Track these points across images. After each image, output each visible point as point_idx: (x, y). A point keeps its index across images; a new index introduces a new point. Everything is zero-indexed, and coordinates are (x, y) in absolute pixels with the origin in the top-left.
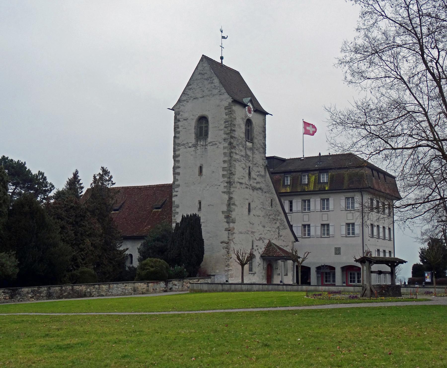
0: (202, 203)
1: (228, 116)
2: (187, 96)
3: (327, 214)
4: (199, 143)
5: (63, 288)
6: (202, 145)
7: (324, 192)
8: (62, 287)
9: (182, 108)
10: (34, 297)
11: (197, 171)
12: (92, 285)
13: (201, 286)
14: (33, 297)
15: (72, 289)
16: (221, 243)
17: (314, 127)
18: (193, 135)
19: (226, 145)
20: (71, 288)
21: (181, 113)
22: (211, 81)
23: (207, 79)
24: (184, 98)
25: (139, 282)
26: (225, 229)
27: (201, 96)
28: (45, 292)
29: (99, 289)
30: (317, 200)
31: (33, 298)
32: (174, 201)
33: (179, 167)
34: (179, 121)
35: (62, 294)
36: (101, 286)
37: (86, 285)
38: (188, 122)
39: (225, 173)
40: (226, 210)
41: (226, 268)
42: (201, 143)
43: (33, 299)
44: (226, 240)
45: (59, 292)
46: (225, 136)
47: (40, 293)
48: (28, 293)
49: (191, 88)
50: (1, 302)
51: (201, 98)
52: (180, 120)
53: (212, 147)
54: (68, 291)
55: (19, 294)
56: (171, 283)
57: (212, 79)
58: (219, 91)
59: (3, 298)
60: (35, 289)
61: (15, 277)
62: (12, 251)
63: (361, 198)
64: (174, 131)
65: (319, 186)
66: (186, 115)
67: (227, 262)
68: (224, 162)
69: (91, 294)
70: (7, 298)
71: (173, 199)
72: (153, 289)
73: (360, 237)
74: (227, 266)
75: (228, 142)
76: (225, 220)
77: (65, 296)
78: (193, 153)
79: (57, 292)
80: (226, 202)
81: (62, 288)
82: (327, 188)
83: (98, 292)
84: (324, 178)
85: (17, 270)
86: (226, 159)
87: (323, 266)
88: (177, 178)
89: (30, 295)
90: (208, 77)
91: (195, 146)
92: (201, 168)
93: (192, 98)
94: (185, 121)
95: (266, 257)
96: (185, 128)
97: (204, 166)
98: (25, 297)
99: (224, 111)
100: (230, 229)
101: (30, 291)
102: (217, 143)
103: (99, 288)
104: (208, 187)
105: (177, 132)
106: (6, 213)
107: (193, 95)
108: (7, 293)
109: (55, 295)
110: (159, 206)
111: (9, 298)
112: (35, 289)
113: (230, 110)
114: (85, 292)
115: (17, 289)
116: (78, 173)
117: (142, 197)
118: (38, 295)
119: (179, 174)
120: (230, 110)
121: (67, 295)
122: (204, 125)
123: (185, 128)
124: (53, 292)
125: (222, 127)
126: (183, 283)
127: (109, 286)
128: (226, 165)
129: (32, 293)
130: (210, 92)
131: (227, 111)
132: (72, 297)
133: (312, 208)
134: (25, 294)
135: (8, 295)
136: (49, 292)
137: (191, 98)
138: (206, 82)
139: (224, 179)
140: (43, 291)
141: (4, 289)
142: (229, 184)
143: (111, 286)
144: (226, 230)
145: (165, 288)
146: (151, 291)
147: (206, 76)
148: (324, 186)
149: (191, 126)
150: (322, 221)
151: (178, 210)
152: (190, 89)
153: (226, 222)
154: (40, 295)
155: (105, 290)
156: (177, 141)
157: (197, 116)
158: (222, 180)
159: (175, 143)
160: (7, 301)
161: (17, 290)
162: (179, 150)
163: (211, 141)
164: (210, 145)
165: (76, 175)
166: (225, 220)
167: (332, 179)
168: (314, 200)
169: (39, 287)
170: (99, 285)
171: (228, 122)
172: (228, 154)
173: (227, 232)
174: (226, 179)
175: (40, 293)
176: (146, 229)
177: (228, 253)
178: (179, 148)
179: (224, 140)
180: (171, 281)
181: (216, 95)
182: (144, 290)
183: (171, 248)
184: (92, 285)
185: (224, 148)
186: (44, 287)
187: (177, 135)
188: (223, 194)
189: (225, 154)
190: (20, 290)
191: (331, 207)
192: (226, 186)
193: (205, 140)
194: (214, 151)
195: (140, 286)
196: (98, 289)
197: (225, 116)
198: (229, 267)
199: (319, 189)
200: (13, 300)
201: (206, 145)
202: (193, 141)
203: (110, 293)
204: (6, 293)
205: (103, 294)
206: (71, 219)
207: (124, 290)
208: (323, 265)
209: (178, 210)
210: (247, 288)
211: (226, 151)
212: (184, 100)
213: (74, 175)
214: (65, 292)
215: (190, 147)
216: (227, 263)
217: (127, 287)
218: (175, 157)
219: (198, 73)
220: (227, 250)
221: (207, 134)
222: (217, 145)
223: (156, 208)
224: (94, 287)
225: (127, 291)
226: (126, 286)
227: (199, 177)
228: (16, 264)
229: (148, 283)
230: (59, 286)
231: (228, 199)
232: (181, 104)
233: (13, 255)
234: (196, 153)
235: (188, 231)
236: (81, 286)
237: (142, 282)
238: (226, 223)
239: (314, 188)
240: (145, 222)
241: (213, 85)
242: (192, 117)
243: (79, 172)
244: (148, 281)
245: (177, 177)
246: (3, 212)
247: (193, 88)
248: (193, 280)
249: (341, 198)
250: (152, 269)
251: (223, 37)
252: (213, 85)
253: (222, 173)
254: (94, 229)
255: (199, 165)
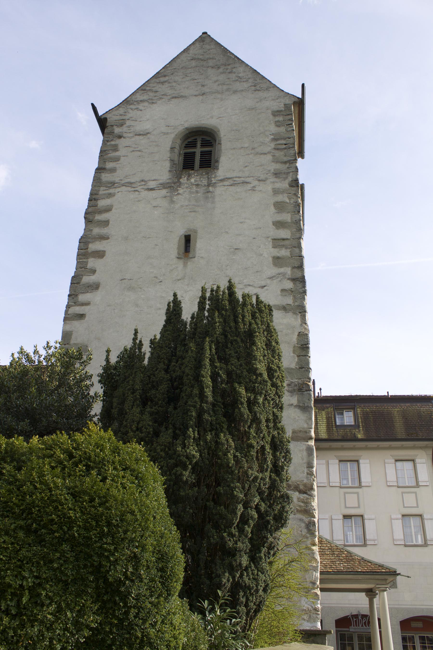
3: (357, 493)
30: (331, 462)
68: (279, 225)
75: (290, 179)
87: (356, 616)
92: (188, 239)
139: (282, 270)
150: (346, 507)
153: (298, 406)
174: (288, 271)
191: (366, 478)
197: (273, 128)
208: (355, 613)
255: (181, 232)
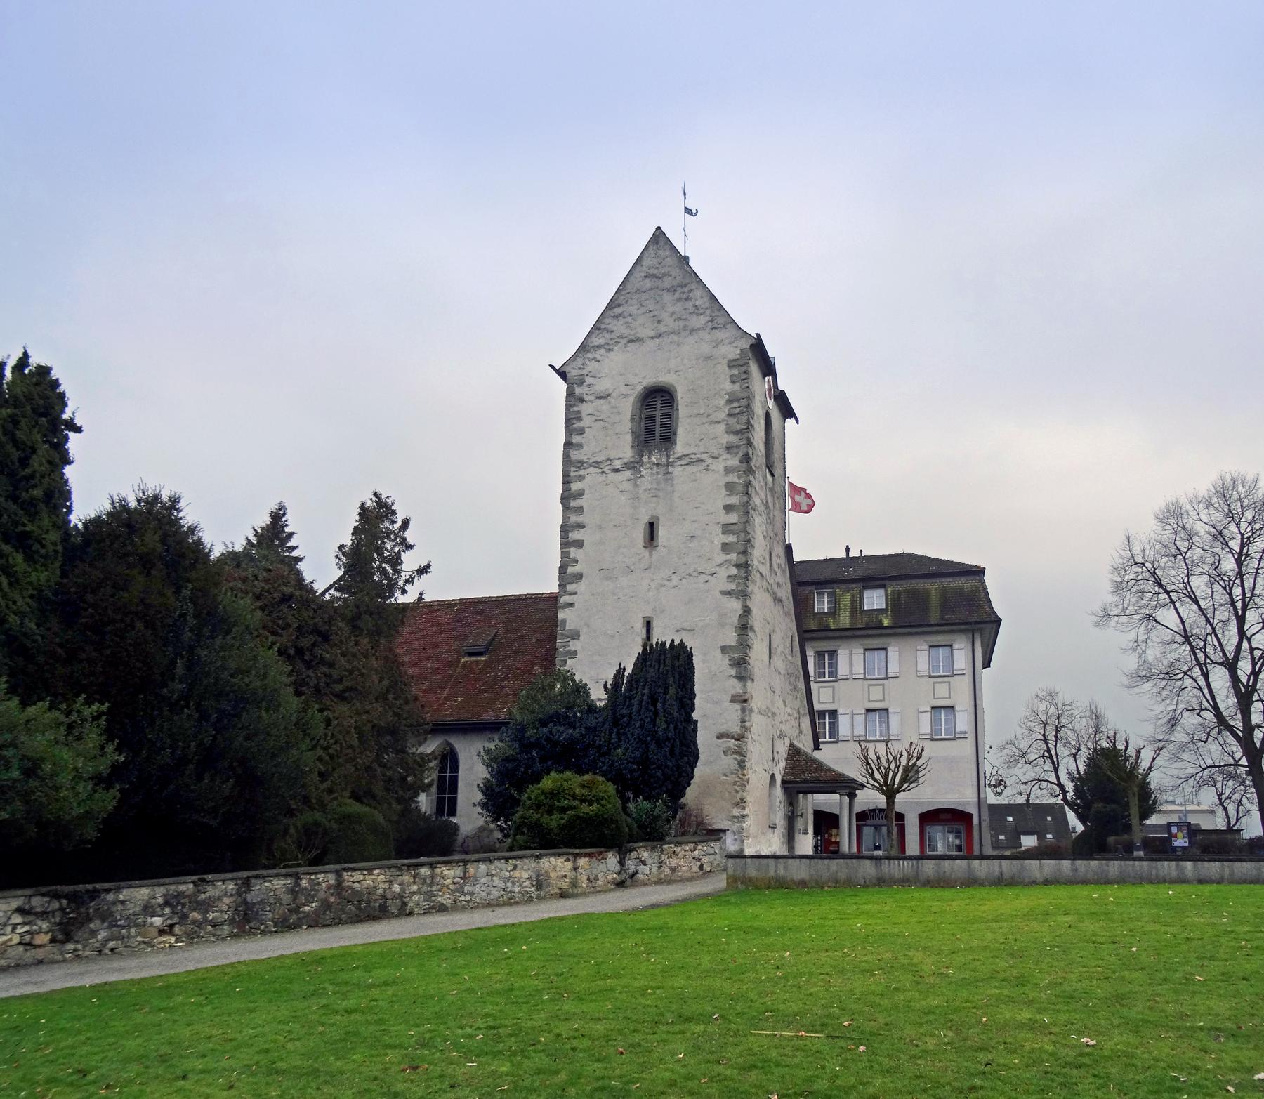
0: (654, 624)
1: (738, 384)
2: (607, 335)
4: (645, 459)
5: (304, 883)
6: (658, 465)
7: (879, 631)
8: (297, 877)
9: (591, 366)
10: (177, 930)
11: (640, 534)
12: (409, 866)
13: (781, 867)
14: (171, 926)
15: (339, 885)
16: (718, 738)
17: (808, 496)
18: (629, 438)
19: (734, 462)
20: (332, 879)
21: (588, 380)
22: (684, 293)
23: (672, 290)
24: (597, 341)
25: (551, 855)
26: (732, 696)
27: (652, 334)
28: (227, 900)
29: (431, 885)
31: (171, 933)
32: (564, 621)
33: (580, 526)
34: (582, 400)
35: (296, 910)
36: (438, 871)
37: (389, 868)
38: (609, 402)
39: (731, 539)
40: (734, 644)
41: (736, 812)
42: (653, 459)
43: (173, 940)
44: (736, 729)
45: (286, 898)
46: (733, 439)
47: (205, 907)
48: (149, 910)
49: (620, 315)
50: (3, 962)
51: (652, 338)
52: (586, 398)
53: (689, 468)
54: (322, 895)
55: (106, 916)
56: (634, 854)
57: (686, 290)
58: (708, 318)
59: (16, 939)
60: (182, 888)
61: (91, 832)
62: (88, 702)
63: (970, 648)
64: (567, 427)
65: (866, 618)
66: (602, 385)
67: (737, 792)
68: (728, 508)
69: (404, 904)
70: (40, 939)
71: (561, 616)
72: (588, 879)
73: (968, 740)
74: (737, 804)
75: (741, 454)
76: (733, 672)
77: (307, 915)
78: (627, 486)
79: (279, 900)
80: (735, 620)
81: (296, 884)
82: (886, 623)
83: (429, 896)
84: (874, 600)
85: (108, 800)
86: (734, 500)
87: (874, 811)
88: (572, 555)
89: (157, 921)
90: (675, 283)
91: (634, 466)
92: (652, 527)
93: (625, 341)
94: (601, 401)
95: (797, 782)
96: (602, 420)
97: (661, 523)
98: (133, 931)
99: (724, 371)
100: (746, 697)
101: (160, 900)
102: (703, 457)
103: (432, 877)
104: (675, 579)
105: (575, 429)
106: (55, 551)
107: (626, 332)
108: (44, 915)
109: (270, 915)
110: (481, 649)
111: (53, 941)
112: (182, 888)
113: (743, 369)
114: (384, 897)
115: (94, 895)
116: (284, 514)
117: (422, 627)
118: (195, 915)
119: (579, 544)
120: (743, 369)
121: (316, 912)
122: (658, 413)
123: (602, 420)
124: (262, 902)
125: (722, 415)
126: (660, 857)
127: (465, 872)
128: (733, 518)
129: (167, 910)
130: (681, 323)
131: (735, 371)
132: (337, 922)
133: (843, 669)
134: (135, 914)
135: (45, 925)
136: (245, 902)
137: (619, 340)
138: (667, 297)
139: (729, 557)
140: (219, 898)
141: (28, 892)
142: (743, 571)
143: (471, 869)
144: (734, 699)
145: (619, 873)
146: (584, 885)
147: (667, 282)
148: (877, 617)
149: (619, 413)
150: (869, 701)
151: (574, 645)
152: (617, 317)
154: (206, 920)
155: (452, 887)
156: (576, 456)
157: (640, 388)
158: (722, 557)
159: (570, 461)
160: (40, 954)
161: (92, 899)
162: (581, 478)
163: (685, 453)
164: (683, 462)
165: (277, 517)
166: (733, 672)
167: (895, 602)
168: (847, 651)
169: (203, 880)
170: (432, 866)
171: (738, 400)
172: (740, 488)
173: (738, 706)
175: (205, 907)
176: (451, 707)
177: (741, 764)
178: (581, 472)
179: (729, 448)
180: (634, 849)
181: (699, 329)
182: (565, 884)
183: (609, 743)
184: (409, 866)
185: (728, 471)
186: (223, 881)
187: (576, 439)
188: (725, 599)
189: (730, 487)
190: (110, 897)
192: (736, 576)
193: (666, 450)
194: (696, 480)
195: (555, 867)
196: (428, 881)
197: (728, 386)
198: (744, 808)
199: (867, 624)
200: (70, 946)
201: (669, 464)
202: (628, 453)
203: (468, 898)
204: (36, 914)
205: (445, 900)
206: (281, 636)
207: (509, 884)
209: (574, 645)
210: (997, 873)
211: (733, 478)
212: (599, 347)
213: (272, 517)
214: (310, 898)
215: (617, 470)
216: (739, 796)
217: (517, 874)
218: (568, 498)
219: (643, 274)
220: (739, 758)
221: (668, 437)
222: (704, 464)
223: (471, 654)
224: (414, 877)
225: (517, 889)
226: (515, 868)
227: (646, 553)
228: (103, 767)
229: (576, 856)
230: (286, 876)
231: (740, 612)
232: (589, 355)
233: (96, 718)
234: (636, 485)
235: (672, 691)
236: (370, 870)
237: (559, 855)
238: (735, 681)
239: (851, 622)
240: (442, 689)
241: (691, 304)
242: (623, 389)
243: (288, 511)
244: (577, 851)
245: (573, 552)
246: (40, 541)
247: (626, 314)
248: (683, 846)
249: (918, 648)
250: (586, 809)
251: (688, 211)
252: (689, 305)
253: (720, 538)
254: (362, 675)
